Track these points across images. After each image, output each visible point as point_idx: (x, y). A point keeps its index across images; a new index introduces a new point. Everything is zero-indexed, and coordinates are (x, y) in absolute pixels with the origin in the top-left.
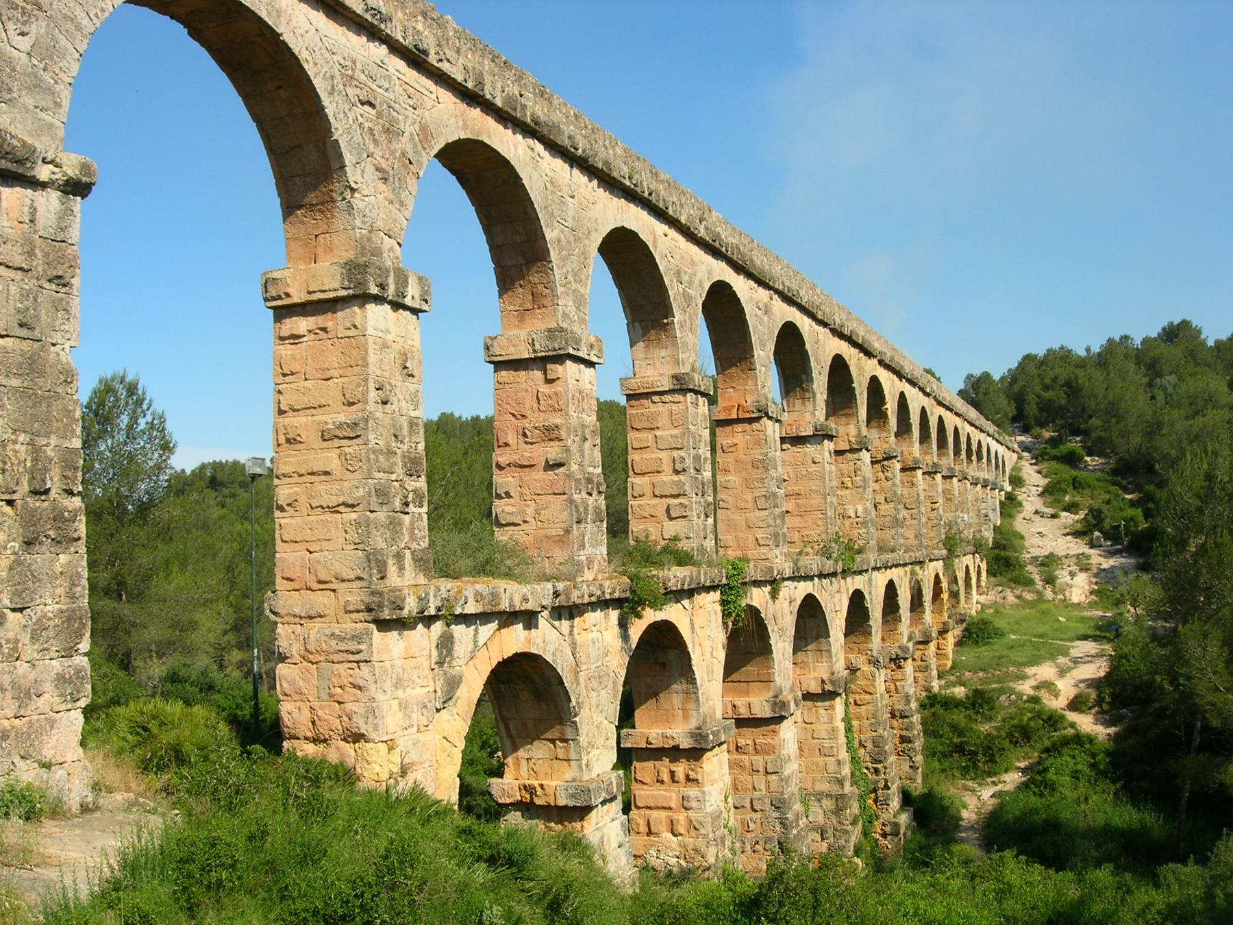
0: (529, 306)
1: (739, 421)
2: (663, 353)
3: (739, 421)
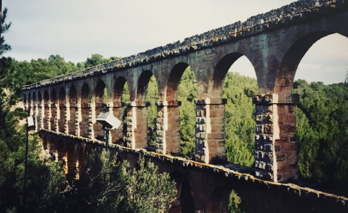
0: (284, 85)
2: (218, 91)
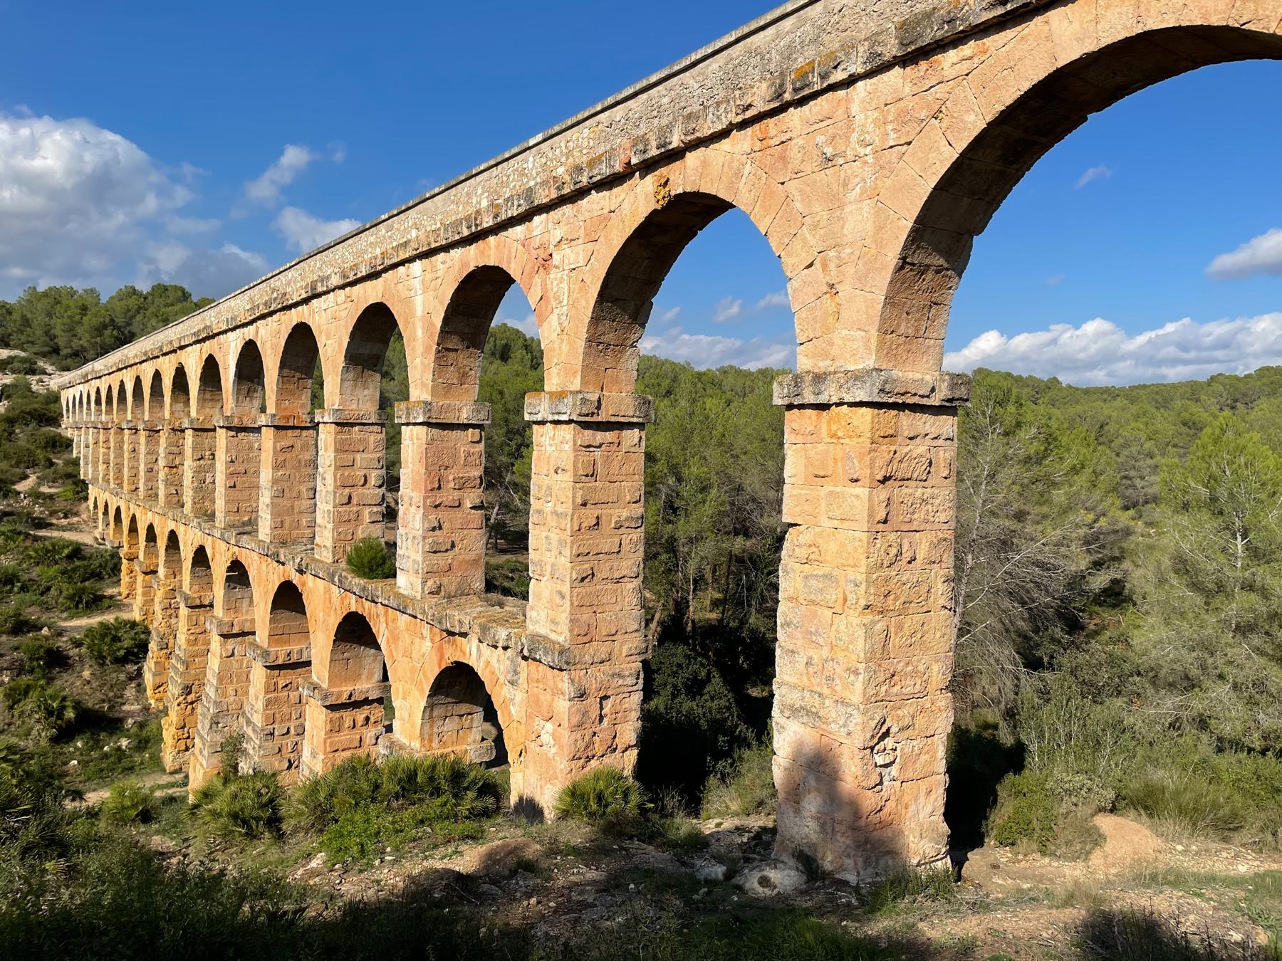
0: (455, 381)
1: (293, 428)
3: (293, 428)
